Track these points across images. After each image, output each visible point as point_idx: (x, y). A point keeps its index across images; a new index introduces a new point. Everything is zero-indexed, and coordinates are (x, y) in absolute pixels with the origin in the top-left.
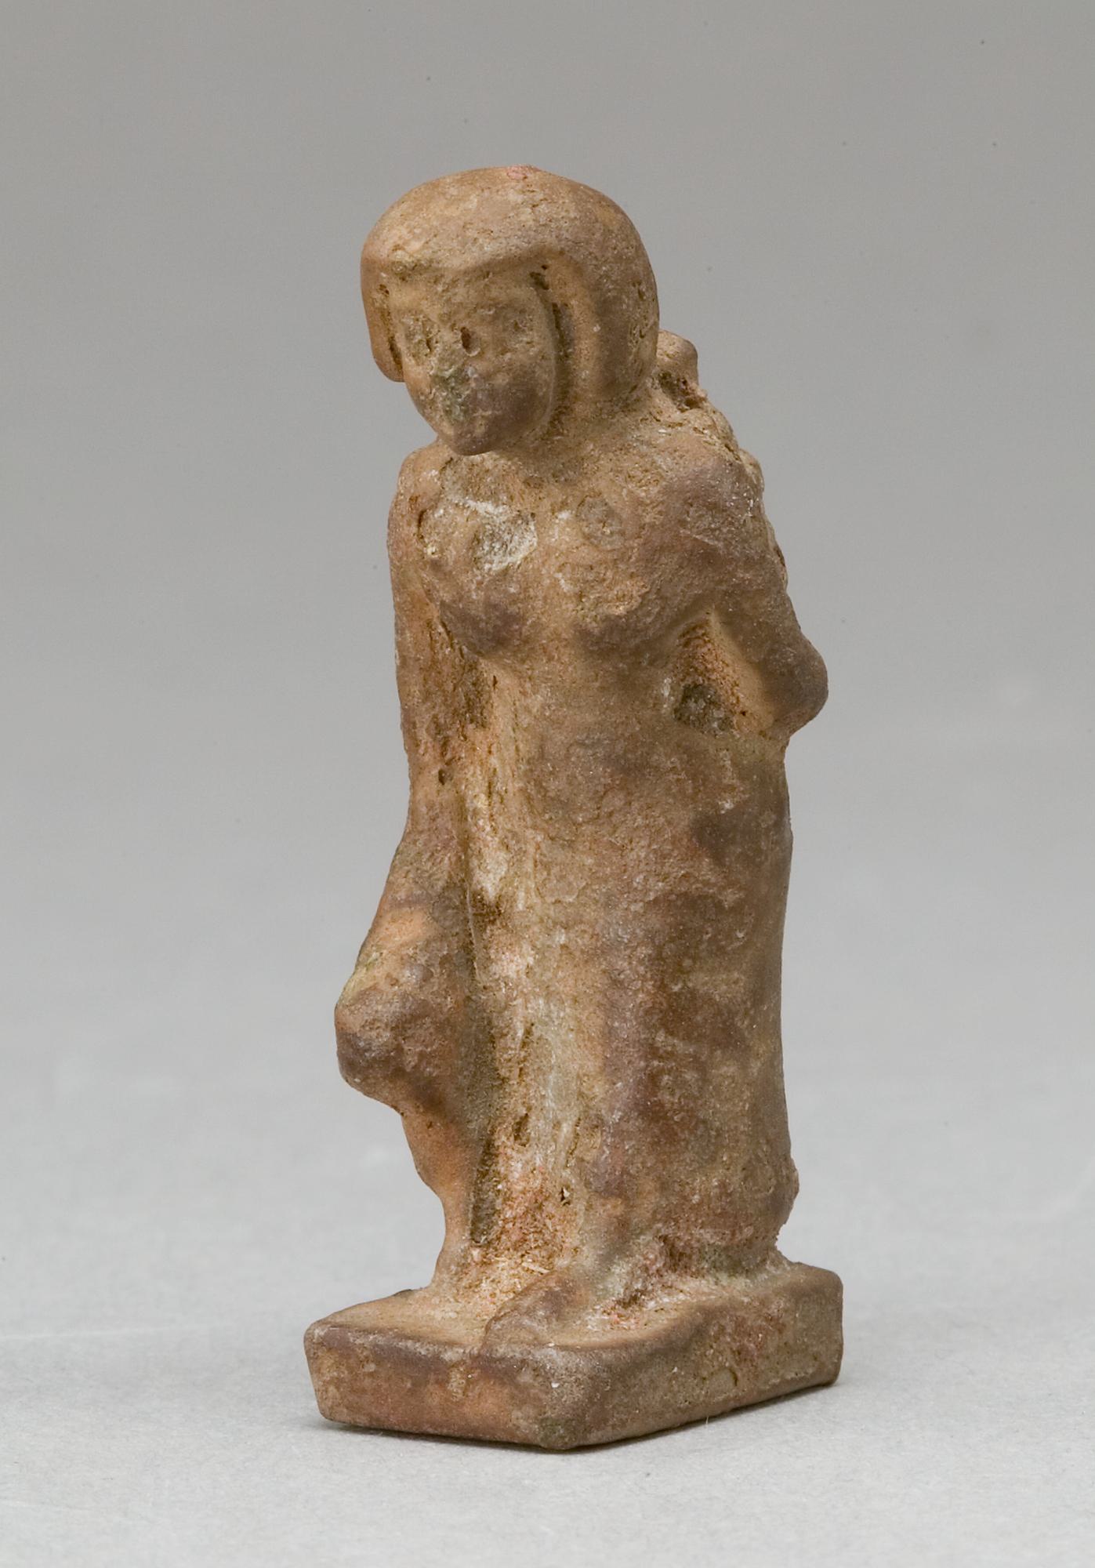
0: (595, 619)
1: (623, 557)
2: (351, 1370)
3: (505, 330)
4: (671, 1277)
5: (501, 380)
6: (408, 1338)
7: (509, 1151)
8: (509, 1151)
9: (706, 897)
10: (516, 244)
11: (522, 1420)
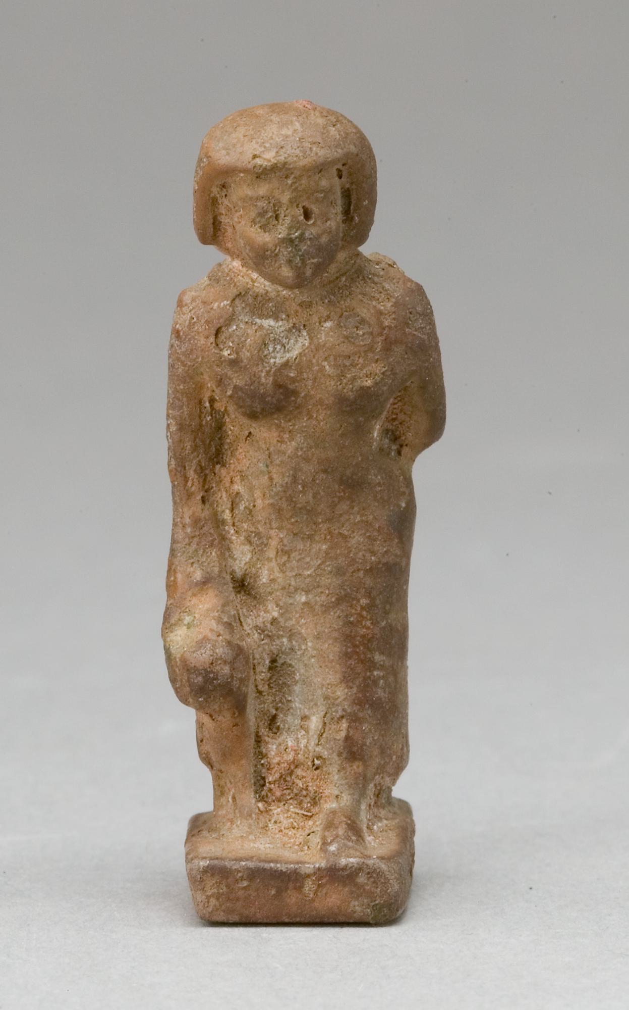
0: (352, 391)
1: (371, 348)
2: (228, 886)
5: (324, 239)
6: (270, 862)
7: (267, 738)
8: (267, 738)
11: (357, 908)
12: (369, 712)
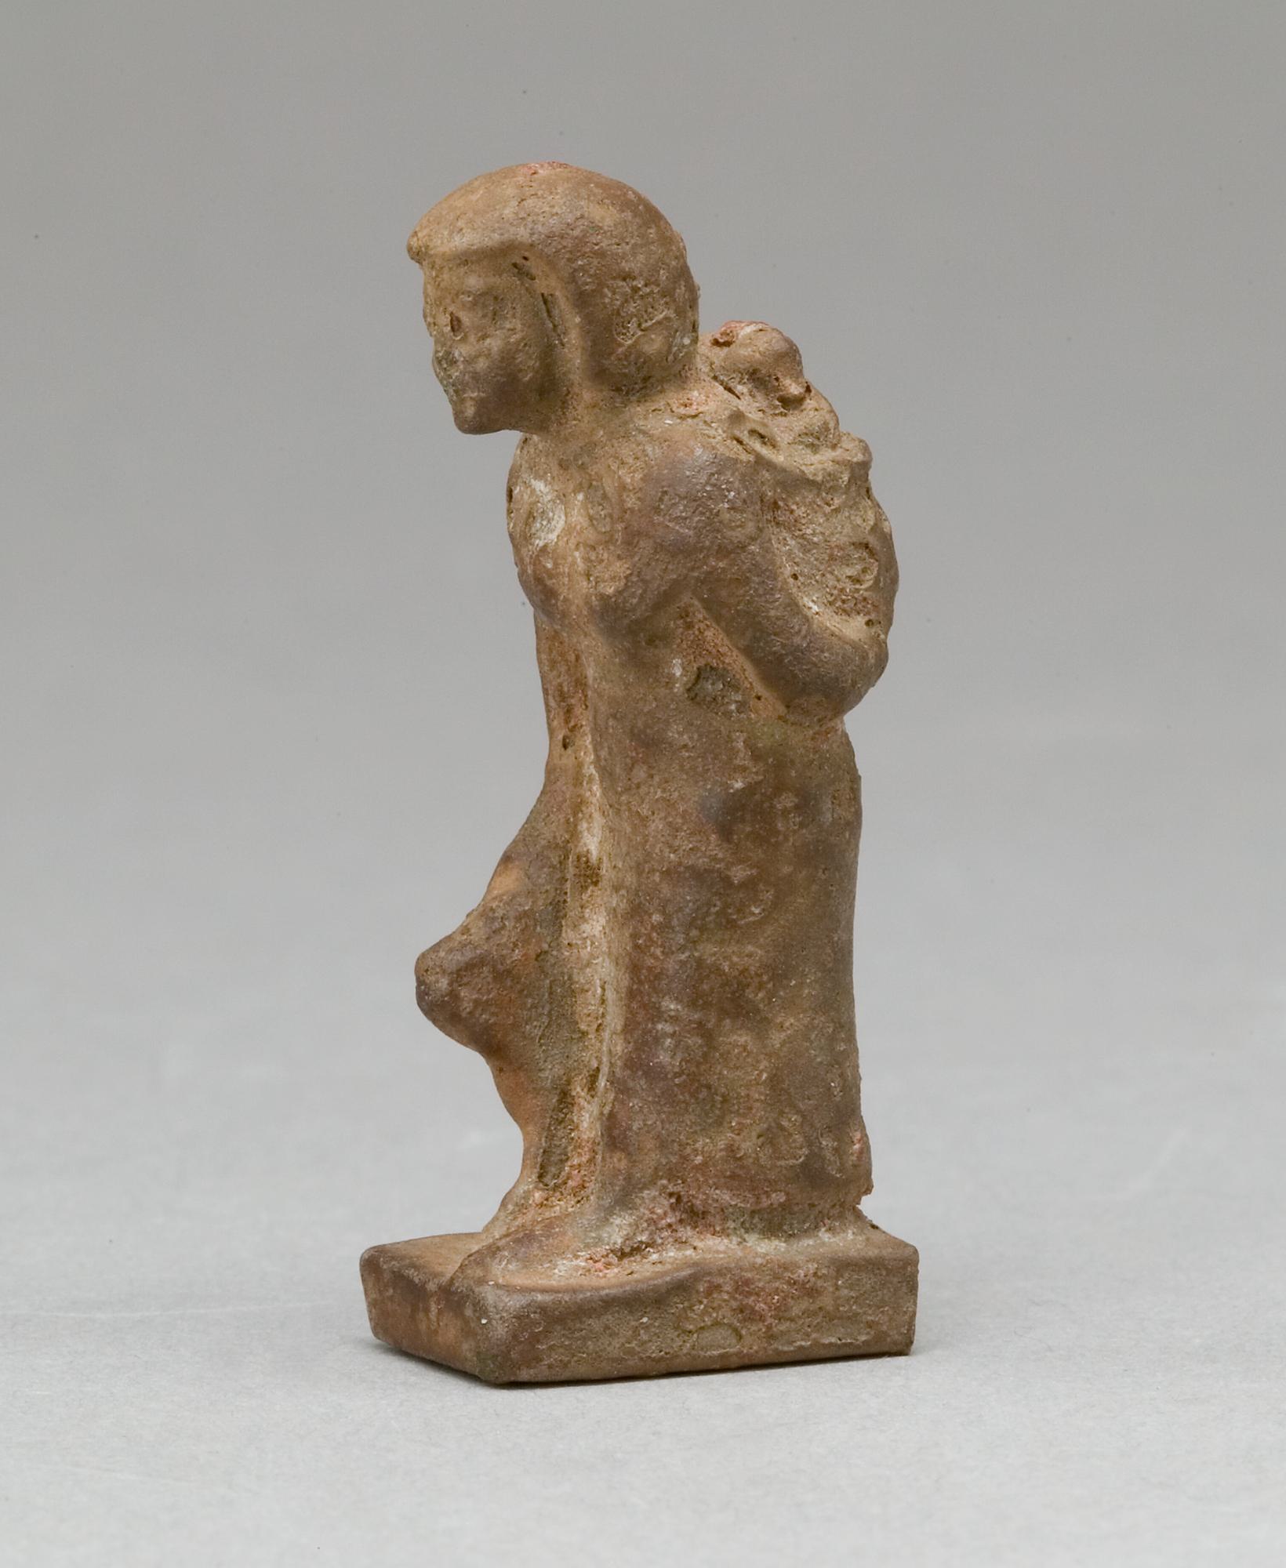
3: (484, 316)
4: (686, 1232)
5: (482, 364)
8: (582, 1102)
9: (712, 871)
10: (494, 239)
12: (642, 1082)
